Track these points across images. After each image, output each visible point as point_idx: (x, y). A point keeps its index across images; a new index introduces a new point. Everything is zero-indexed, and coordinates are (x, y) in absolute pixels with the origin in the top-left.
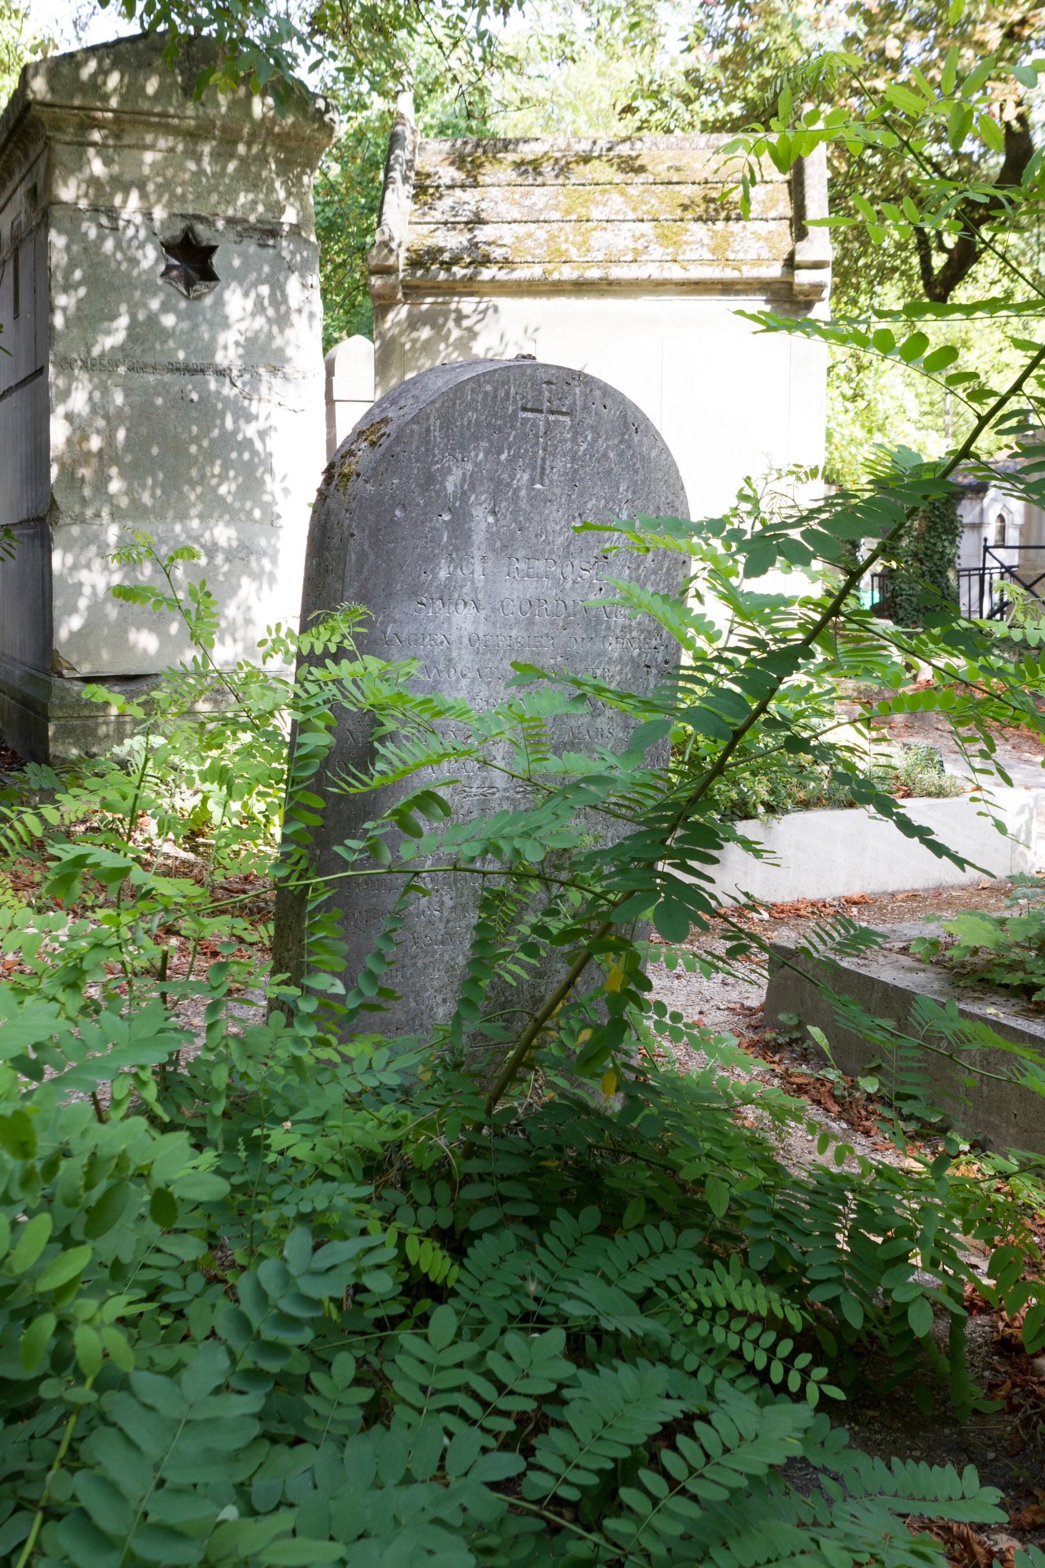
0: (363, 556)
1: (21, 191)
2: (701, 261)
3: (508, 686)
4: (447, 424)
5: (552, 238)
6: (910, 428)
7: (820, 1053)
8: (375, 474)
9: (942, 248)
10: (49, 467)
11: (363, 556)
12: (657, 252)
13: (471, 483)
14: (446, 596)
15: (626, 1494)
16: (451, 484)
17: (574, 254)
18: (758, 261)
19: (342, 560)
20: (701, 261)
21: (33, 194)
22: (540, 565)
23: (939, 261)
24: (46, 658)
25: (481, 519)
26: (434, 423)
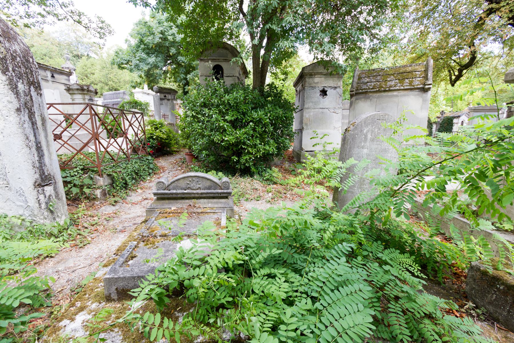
0: (350, 142)
1: (301, 85)
2: (407, 86)
3: (321, 58)
4: (365, 123)
5: (380, 84)
6: (444, 107)
7: (420, 217)
8: (353, 130)
9: (455, 75)
10: (259, 59)
11: (350, 142)
12: (399, 85)
13: (368, 131)
14: (363, 147)
15: (385, 288)
16: (365, 131)
17: (384, 86)
18: (418, 85)
19: (347, 143)
20: (407, 86)
21: (302, 85)
22: (378, 143)
23: (453, 77)
24: (301, 149)
25: (369, 136)
26: (363, 123)
